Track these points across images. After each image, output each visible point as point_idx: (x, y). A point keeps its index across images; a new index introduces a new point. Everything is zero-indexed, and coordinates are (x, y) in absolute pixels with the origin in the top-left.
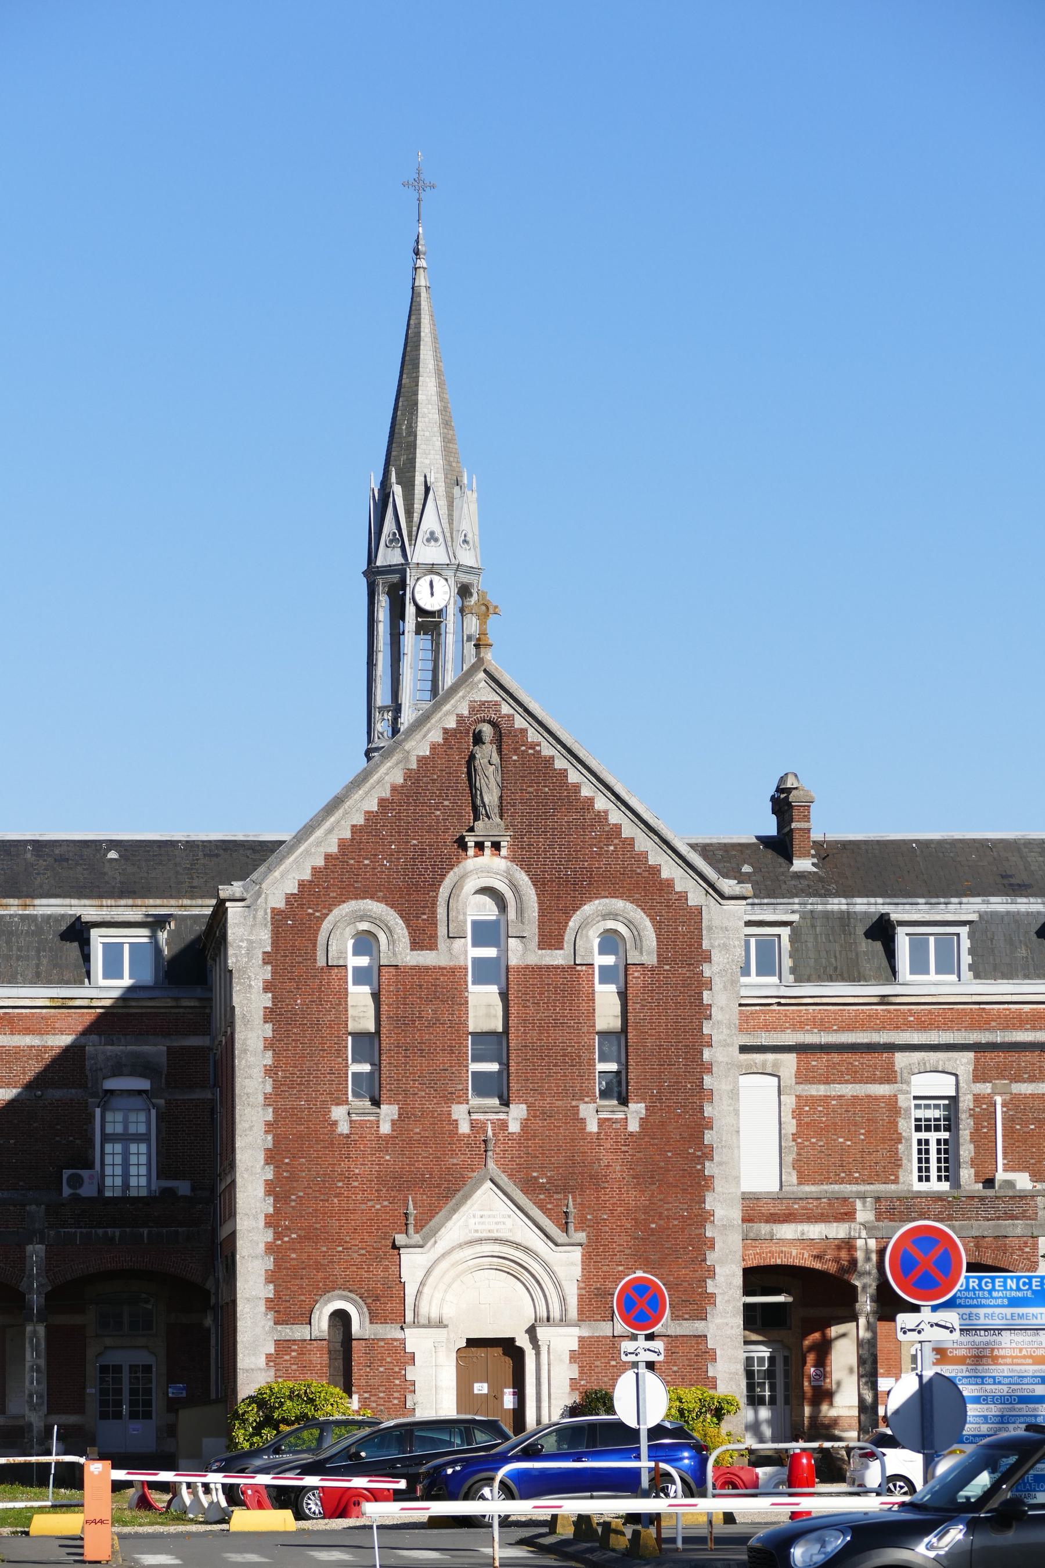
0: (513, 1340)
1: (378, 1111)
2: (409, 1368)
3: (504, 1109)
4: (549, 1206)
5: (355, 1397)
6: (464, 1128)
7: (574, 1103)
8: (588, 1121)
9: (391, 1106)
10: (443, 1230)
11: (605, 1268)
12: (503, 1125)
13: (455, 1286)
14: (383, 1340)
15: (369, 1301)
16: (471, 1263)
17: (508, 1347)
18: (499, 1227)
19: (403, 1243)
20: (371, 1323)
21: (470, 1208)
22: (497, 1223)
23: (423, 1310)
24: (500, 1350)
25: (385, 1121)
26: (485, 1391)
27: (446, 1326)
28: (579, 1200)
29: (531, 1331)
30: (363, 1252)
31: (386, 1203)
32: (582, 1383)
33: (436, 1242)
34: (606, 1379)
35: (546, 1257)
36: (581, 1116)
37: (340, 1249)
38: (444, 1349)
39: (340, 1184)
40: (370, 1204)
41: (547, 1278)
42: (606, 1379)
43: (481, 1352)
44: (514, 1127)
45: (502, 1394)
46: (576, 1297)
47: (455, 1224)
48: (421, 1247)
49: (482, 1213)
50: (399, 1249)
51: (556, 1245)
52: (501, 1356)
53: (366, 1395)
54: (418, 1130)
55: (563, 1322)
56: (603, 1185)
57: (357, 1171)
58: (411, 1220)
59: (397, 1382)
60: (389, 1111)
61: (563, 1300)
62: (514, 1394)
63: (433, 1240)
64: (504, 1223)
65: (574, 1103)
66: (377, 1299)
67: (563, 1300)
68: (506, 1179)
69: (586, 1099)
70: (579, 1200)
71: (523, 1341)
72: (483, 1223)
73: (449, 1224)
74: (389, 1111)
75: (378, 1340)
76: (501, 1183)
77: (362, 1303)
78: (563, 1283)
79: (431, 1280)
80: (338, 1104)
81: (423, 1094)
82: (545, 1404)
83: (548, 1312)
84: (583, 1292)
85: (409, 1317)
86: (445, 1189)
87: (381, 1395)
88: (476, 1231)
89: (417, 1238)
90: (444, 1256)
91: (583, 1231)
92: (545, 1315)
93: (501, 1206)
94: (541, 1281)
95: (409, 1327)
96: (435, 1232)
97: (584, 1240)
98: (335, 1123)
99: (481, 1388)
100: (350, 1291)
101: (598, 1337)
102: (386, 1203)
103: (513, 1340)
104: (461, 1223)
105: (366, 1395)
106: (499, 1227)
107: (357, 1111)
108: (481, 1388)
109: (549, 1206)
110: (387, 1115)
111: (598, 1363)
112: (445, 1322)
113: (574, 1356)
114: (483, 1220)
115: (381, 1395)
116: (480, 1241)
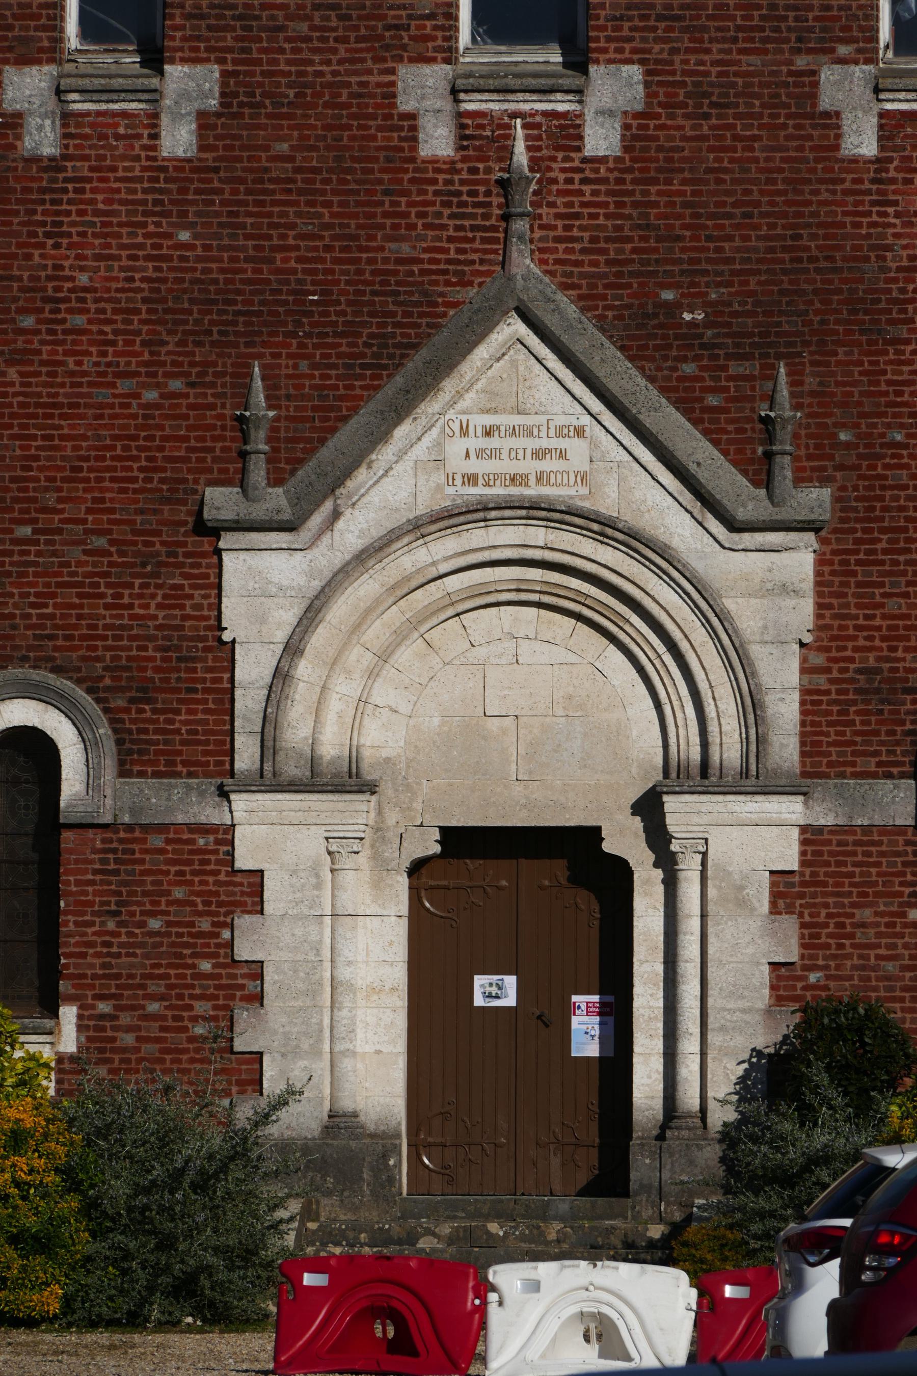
0: (593, 834)
1: (155, 82)
2: (243, 922)
3: (572, 80)
4: (713, 400)
5: (69, 1014)
6: (437, 141)
7: (801, 62)
8: (847, 122)
9: (199, 69)
10: (362, 475)
11: (893, 605)
12: (568, 131)
13: (405, 655)
14: (162, 828)
15: (120, 702)
16: (454, 583)
17: (577, 850)
18: (547, 465)
19: (227, 514)
20: (123, 773)
21: (453, 403)
22: (539, 454)
23: (297, 729)
24: (559, 868)
25: (177, 117)
26: (510, 1000)
27: (370, 788)
28: (811, 382)
29: (649, 808)
30: (101, 542)
31: (176, 385)
32: (813, 977)
33: (336, 515)
34: (890, 967)
35: (698, 566)
36: (825, 103)
37: (27, 531)
38: (363, 859)
39: (28, 322)
40: (124, 386)
41: (700, 635)
42: (890, 967)
43: (498, 874)
44: (601, 140)
45: (568, 1010)
46: (795, 697)
47: (400, 456)
48: (289, 527)
49: (489, 420)
50: (215, 532)
51: (733, 526)
52: (527, 895)
53: (104, 1007)
54: (284, 147)
55: (754, 779)
56: (892, 332)
57: (83, 279)
58: (260, 442)
59: (206, 966)
60: (190, 85)
61: (753, 707)
62: (604, 1011)
63: (328, 505)
64: (562, 455)
65: (801, 62)
66: (144, 694)
67: (753, 707)
68: (572, 311)
69: (843, 50)
70: (811, 382)
71: (625, 840)
72: (494, 454)
73: (384, 455)
74: (190, 85)
75: (148, 828)
76: (551, 321)
77: (95, 709)
78: (756, 651)
79: (319, 640)
80: (24, 61)
81: (304, 27)
82: (689, 1046)
83: (705, 744)
84: (821, 681)
85: (246, 755)
86: (372, 351)
87: (153, 1007)
88: (471, 479)
89: (276, 500)
90: (364, 558)
91: (824, 481)
92: (695, 754)
93: (551, 396)
94: (684, 646)
95: (246, 788)
96: (335, 481)
97: (825, 514)
98: (14, 122)
99: (496, 991)
100: (57, 670)
101: (867, 829)
102: (176, 385)
103: (593, 834)
104: (420, 451)
105: (104, 1007)
106: (547, 465)
107: (86, 83)
108: (496, 991)
109: (713, 400)
110: (184, 95)
111: (866, 915)
112: (369, 774)
113: (784, 890)
114: (494, 442)
115: (153, 1007)
116: (481, 512)
